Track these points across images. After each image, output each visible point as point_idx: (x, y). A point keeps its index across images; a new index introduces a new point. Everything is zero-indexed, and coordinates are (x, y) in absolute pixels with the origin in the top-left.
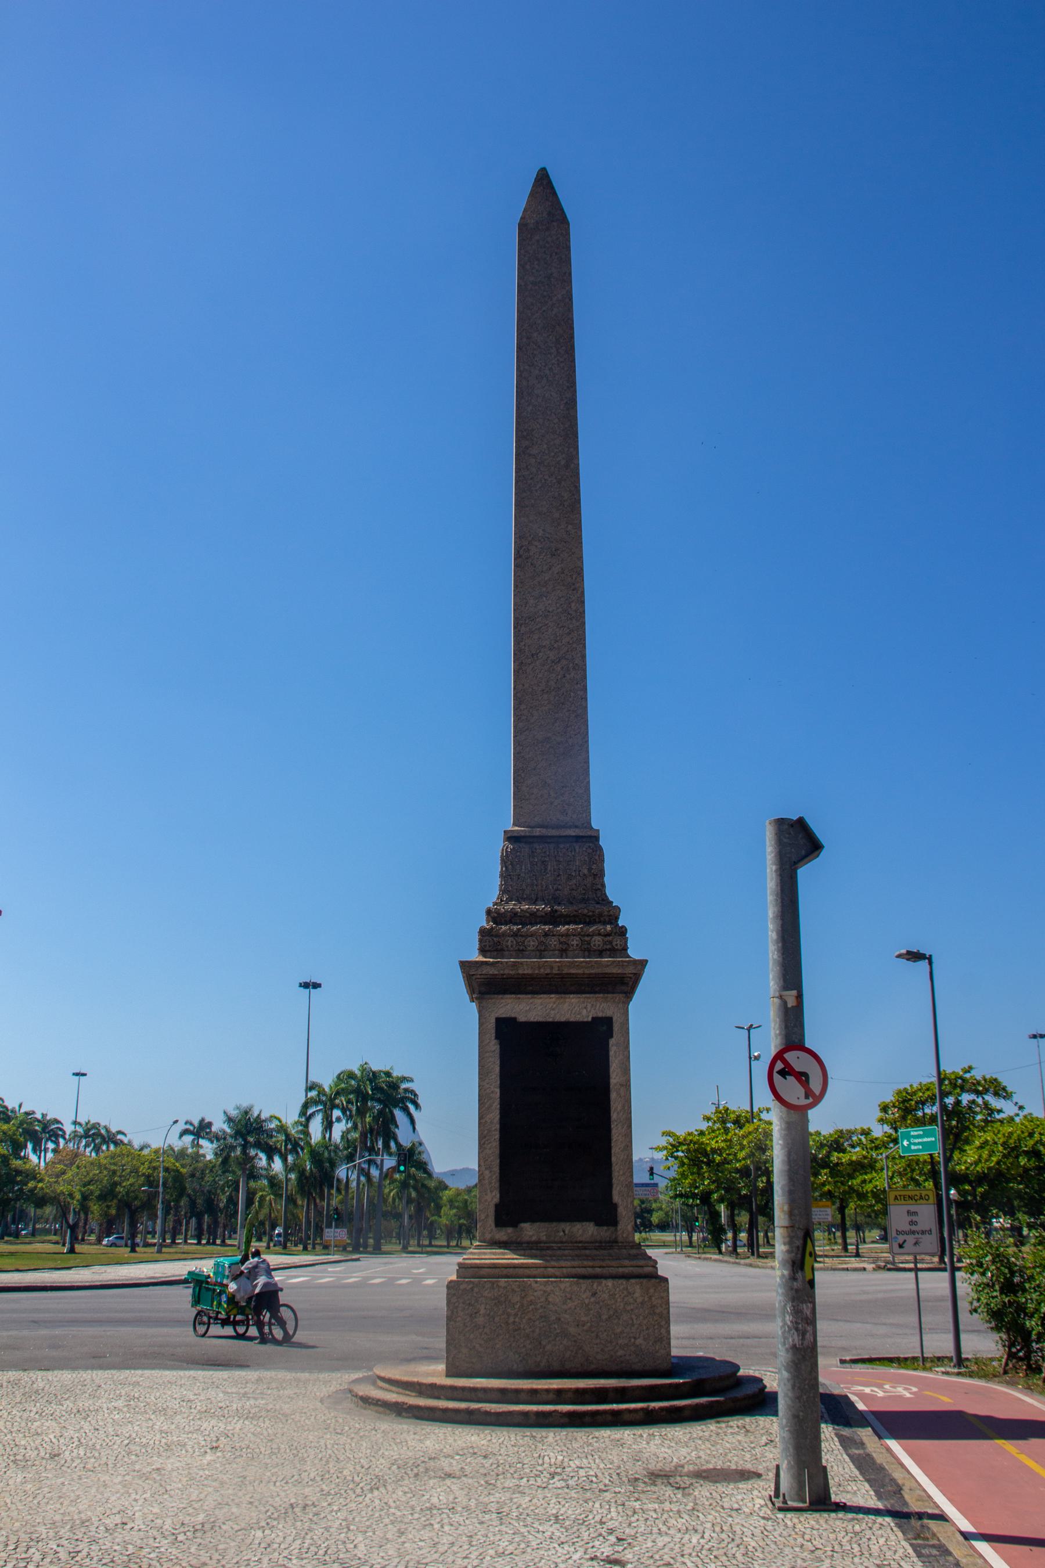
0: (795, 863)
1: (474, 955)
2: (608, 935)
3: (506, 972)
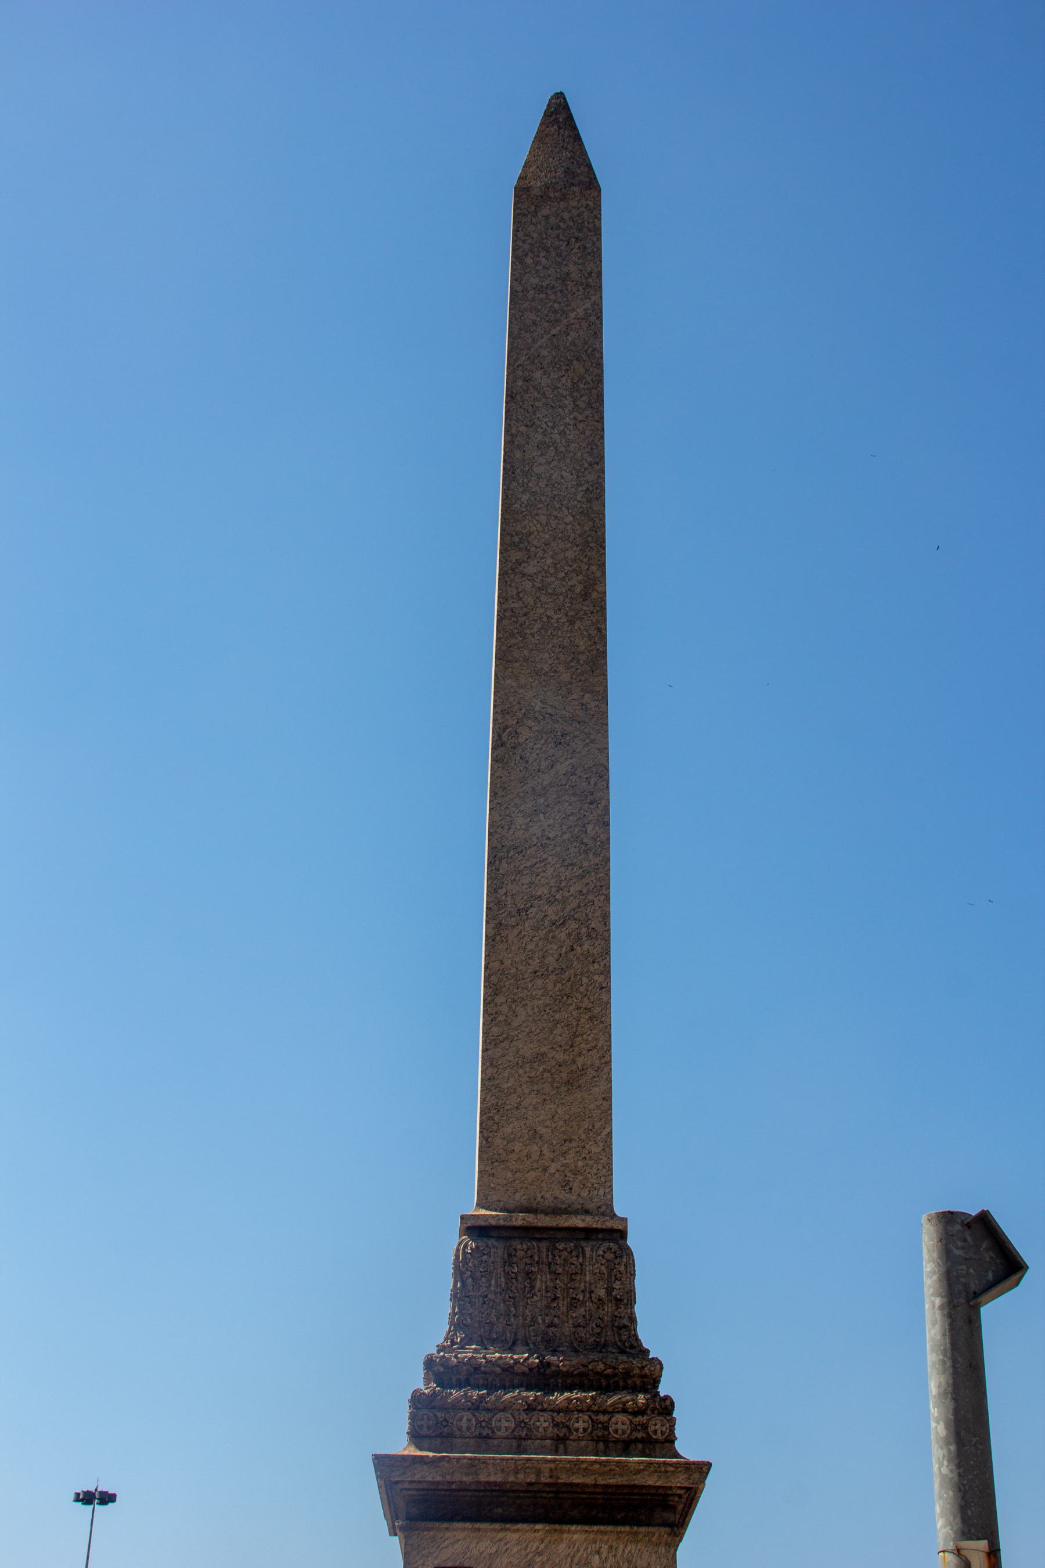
0: (976, 1295)
1: (400, 1445)
2: (640, 1412)
3: (457, 1477)
